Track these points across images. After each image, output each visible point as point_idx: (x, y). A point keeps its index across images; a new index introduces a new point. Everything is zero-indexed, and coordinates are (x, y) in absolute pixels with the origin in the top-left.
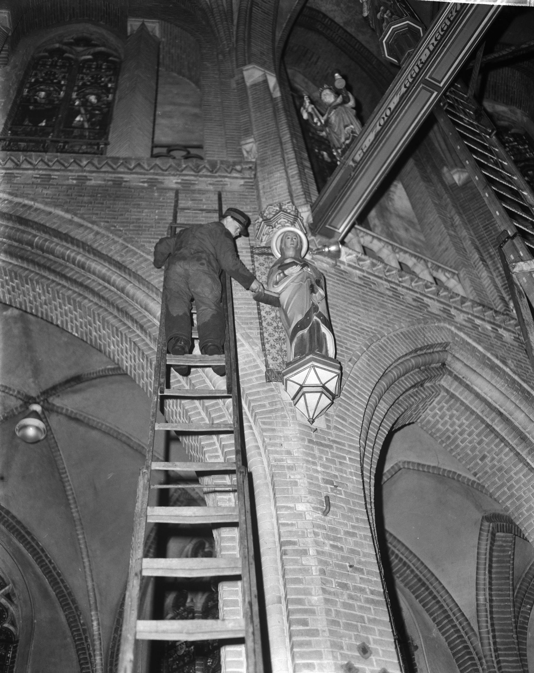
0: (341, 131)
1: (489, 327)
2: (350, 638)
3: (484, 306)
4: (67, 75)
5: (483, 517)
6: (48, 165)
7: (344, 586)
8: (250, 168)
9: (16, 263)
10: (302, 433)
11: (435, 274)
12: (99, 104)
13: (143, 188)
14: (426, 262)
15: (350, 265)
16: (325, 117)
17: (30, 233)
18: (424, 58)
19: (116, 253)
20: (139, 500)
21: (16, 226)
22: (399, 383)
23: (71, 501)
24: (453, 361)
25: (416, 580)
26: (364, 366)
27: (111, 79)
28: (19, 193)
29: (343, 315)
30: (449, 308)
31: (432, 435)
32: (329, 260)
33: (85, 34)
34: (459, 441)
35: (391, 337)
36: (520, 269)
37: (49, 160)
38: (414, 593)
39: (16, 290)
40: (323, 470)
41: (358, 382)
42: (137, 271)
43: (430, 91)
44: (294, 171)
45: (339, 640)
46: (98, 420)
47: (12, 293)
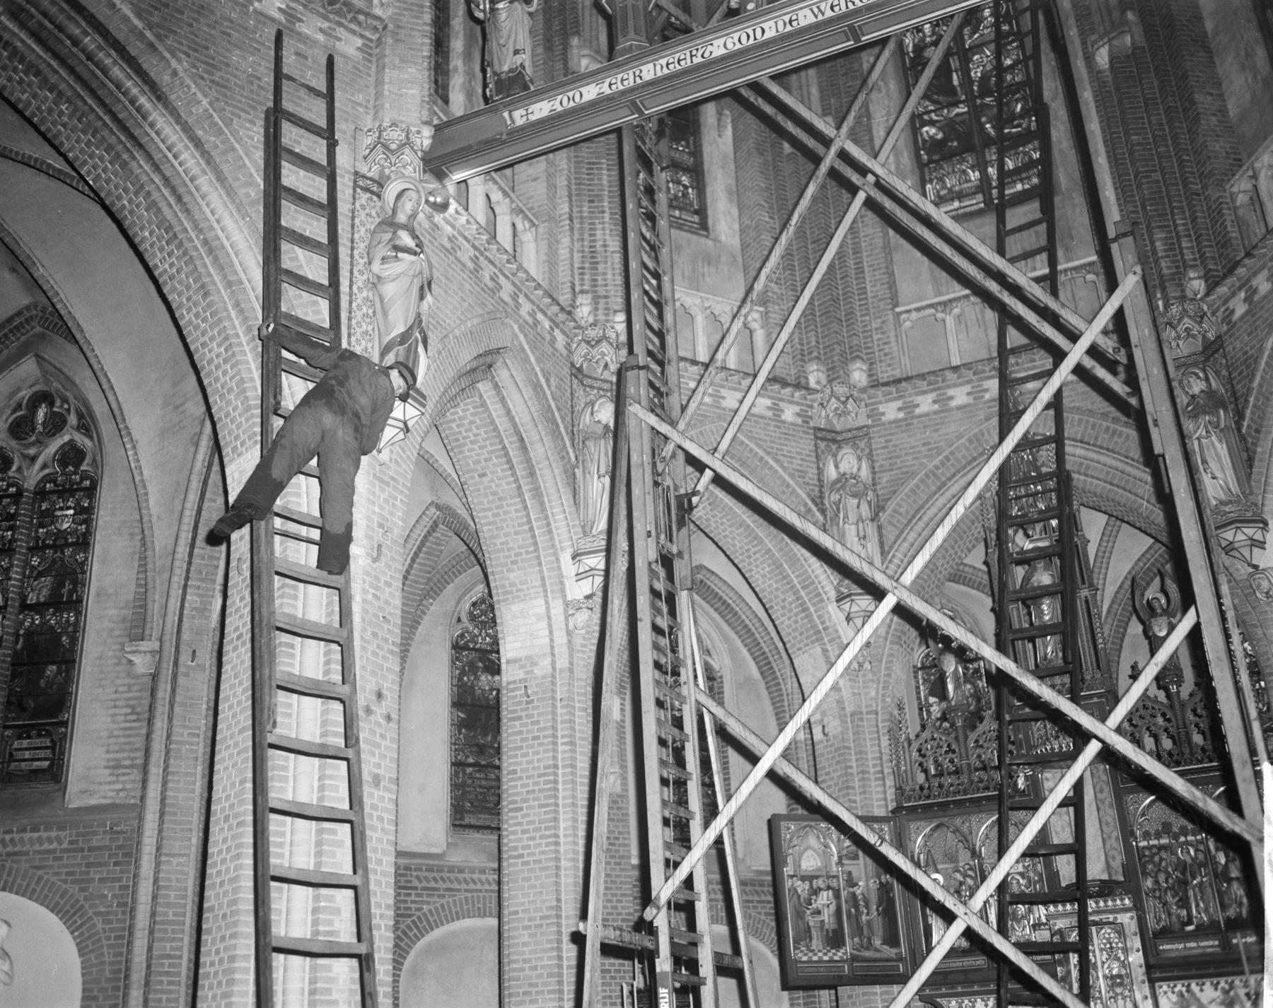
1: (547, 324)
3: (553, 299)
14: (512, 201)
17: (79, 25)
34: (466, 449)
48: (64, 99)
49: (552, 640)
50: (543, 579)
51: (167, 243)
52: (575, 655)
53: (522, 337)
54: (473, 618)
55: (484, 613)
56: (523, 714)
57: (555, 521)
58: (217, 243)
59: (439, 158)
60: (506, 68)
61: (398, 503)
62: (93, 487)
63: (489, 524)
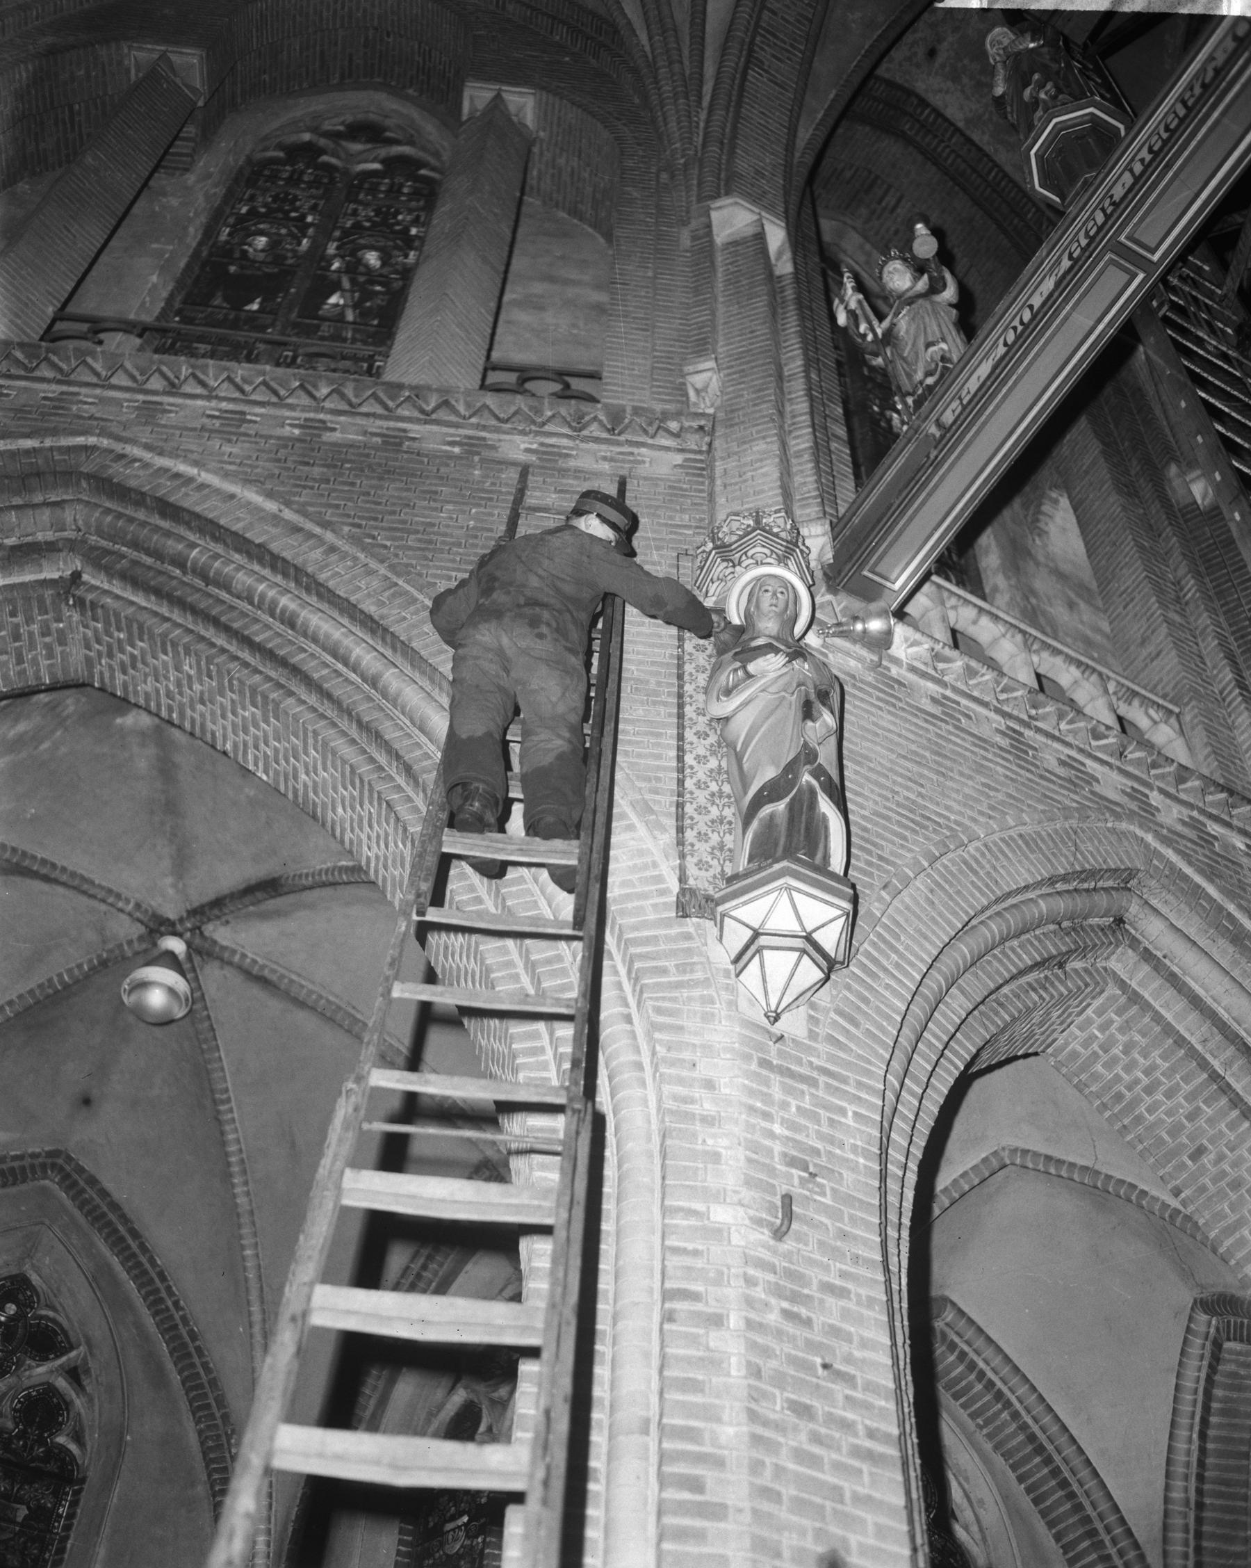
0: (917, 354)
2: (802, 1533)
3: (1231, 792)
4: (322, 203)
6: (242, 391)
7: (803, 1411)
8: (701, 428)
9: (144, 604)
11: (1123, 709)
12: (385, 271)
13: (450, 456)
15: (913, 669)
16: (886, 323)
17: (181, 538)
18: (1118, 192)
19: (369, 595)
20: (329, 1153)
21: (151, 520)
22: (1003, 952)
23: (235, 1169)
24: (1141, 916)
25: (1021, 1437)
26: (918, 903)
27: (418, 217)
28: (168, 446)
29: (882, 780)
30: (1147, 791)
31: (1079, 1087)
32: (864, 653)
33: (372, 117)
35: (995, 844)
37: (244, 380)
38: (1014, 1467)
39: (140, 665)
40: (787, 1133)
41: (898, 938)
42: (410, 640)
43: (1126, 270)
44: (802, 442)
45: (775, 1537)
46: (311, 986)
47: (131, 671)
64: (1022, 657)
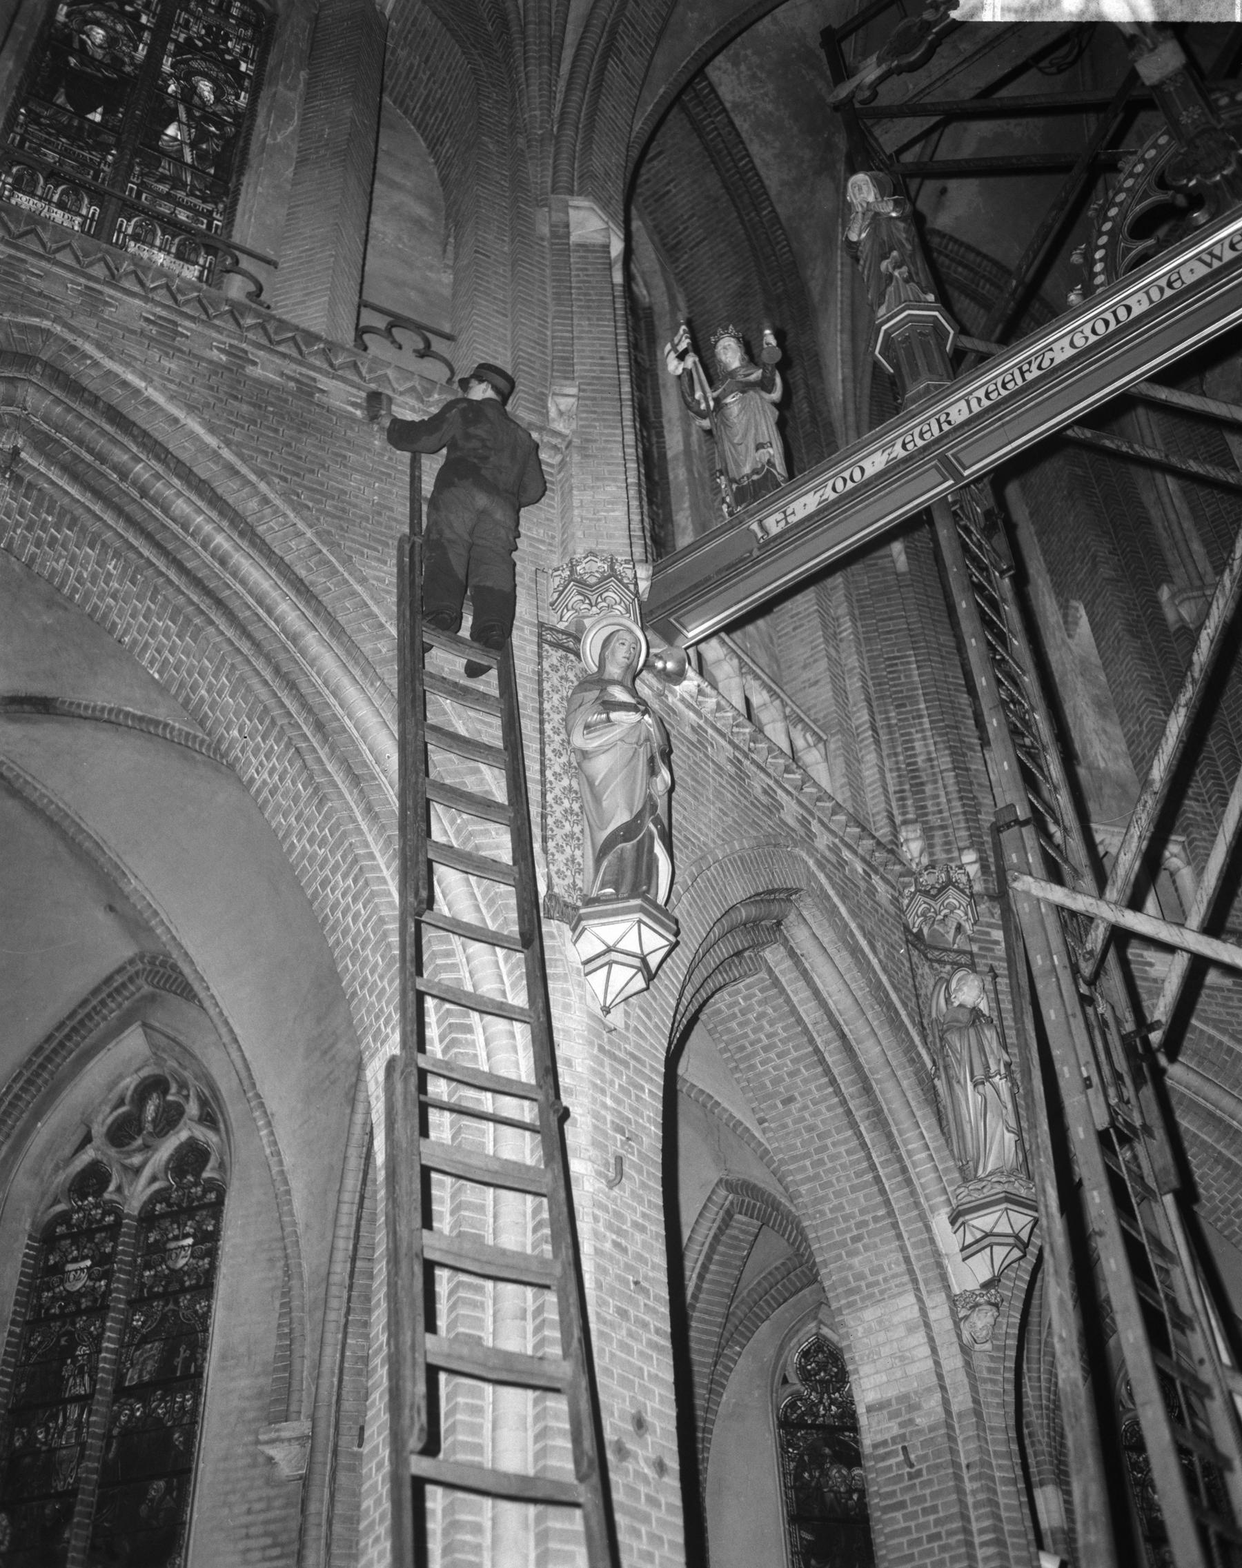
1: (859, 867)
3: (864, 829)
5: (721, 1180)
6: (176, 300)
10: (590, 1029)
13: (353, 419)
14: (784, 705)
17: (126, 449)
28: (113, 346)
34: (757, 1060)
36: (1025, 888)
37: (178, 289)
48: (111, 553)
49: (937, 1363)
50: (907, 1260)
51: (264, 739)
52: (981, 1387)
53: (822, 877)
54: (806, 1376)
55: (822, 1367)
56: (907, 1497)
57: (915, 1165)
58: (335, 724)
59: (664, 605)
60: (747, 470)
61: (646, 1096)
62: (220, 1202)
63: (809, 1179)
64: (735, 682)
